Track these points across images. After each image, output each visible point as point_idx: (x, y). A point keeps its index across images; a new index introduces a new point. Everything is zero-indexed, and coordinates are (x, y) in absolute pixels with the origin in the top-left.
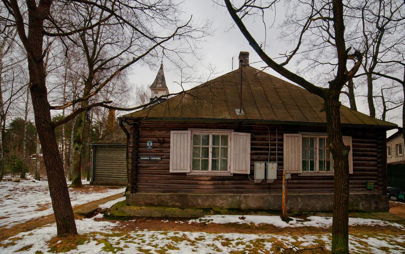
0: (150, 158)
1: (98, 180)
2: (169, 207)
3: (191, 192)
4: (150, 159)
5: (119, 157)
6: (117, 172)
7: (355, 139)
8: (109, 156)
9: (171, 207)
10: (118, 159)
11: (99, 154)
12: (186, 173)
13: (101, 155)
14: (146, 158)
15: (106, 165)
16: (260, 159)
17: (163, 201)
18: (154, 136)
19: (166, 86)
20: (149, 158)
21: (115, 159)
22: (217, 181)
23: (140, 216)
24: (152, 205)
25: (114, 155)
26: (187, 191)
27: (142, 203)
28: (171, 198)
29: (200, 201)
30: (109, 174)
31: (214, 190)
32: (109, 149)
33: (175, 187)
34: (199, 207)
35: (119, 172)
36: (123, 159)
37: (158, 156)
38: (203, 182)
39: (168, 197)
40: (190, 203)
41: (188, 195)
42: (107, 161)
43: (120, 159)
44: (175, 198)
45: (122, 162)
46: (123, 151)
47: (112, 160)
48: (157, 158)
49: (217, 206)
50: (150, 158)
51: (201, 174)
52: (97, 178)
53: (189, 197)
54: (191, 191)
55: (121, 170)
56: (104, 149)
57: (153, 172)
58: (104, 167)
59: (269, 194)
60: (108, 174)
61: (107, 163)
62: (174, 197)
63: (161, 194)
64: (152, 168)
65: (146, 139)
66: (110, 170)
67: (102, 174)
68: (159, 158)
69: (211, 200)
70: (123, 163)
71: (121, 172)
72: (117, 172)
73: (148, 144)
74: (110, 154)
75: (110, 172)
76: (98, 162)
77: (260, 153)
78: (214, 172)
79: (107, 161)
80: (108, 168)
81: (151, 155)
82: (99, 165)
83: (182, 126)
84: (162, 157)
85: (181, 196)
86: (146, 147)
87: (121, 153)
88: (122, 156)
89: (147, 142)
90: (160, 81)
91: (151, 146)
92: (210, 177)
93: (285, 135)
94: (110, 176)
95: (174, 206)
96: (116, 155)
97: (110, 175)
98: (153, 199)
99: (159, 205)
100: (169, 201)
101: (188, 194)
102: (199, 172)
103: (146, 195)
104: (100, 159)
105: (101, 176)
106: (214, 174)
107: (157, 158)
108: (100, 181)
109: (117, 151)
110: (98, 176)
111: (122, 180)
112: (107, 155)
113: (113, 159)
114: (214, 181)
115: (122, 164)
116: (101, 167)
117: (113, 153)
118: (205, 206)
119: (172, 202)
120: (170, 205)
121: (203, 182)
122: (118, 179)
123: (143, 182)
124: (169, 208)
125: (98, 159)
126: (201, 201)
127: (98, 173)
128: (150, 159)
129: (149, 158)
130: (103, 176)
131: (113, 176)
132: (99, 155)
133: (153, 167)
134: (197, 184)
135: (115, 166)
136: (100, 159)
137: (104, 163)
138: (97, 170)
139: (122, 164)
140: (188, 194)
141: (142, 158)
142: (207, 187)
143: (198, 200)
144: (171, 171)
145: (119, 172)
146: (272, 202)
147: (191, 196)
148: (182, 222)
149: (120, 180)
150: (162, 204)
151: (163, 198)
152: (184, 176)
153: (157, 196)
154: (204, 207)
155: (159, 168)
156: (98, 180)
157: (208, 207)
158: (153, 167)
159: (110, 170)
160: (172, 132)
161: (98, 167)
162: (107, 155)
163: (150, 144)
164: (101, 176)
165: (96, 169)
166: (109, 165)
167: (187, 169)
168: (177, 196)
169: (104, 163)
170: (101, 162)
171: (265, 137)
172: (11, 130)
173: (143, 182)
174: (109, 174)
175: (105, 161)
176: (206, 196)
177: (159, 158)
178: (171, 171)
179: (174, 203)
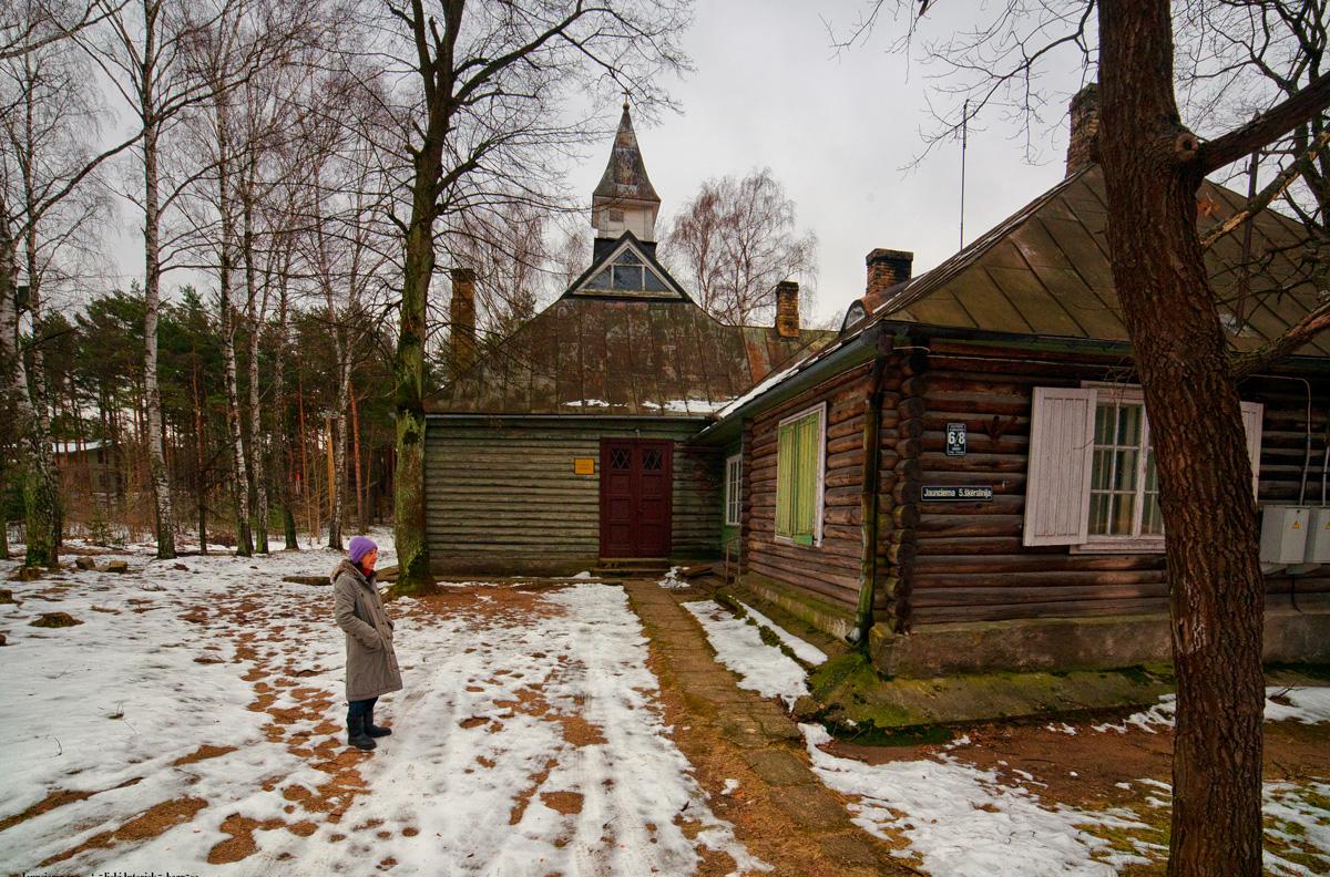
0: (957, 493)
1: (439, 554)
2: (1018, 671)
3: (1080, 612)
4: (957, 496)
5: (518, 466)
6: (515, 523)
7: (1277, 416)
8: (480, 462)
9: (1025, 672)
10: (517, 474)
11: (439, 453)
12: (1068, 546)
13: (448, 458)
14: (944, 493)
15: (467, 497)
16: (1276, 493)
17: (1001, 654)
18: (972, 407)
19: (652, 192)
20: (953, 494)
21: (502, 474)
22: (1149, 573)
23: (968, 718)
24: (964, 670)
25: (501, 459)
26: (1067, 610)
27: (932, 666)
28: (1027, 638)
29: (1110, 642)
30: (485, 531)
31: (1141, 601)
32: (480, 433)
33: (1030, 599)
34: (1106, 664)
35: (521, 523)
36: (535, 475)
37: (983, 483)
38: (1110, 576)
39: (1018, 637)
40: (1081, 654)
41: (1077, 625)
42: (473, 481)
43: (525, 474)
44: (1039, 639)
45: (529, 483)
46: (534, 444)
47: (492, 478)
48: (980, 493)
49: (1156, 658)
50: (957, 493)
51: (1112, 547)
52: (436, 546)
53: (1079, 633)
54: (1078, 610)
55: (529, 515)
56: (458, 435)
57: (966, 544)
58: (462, 507)
59: (1292, 613)
60: (477, 531)
61: (474, 490)
62: (1036, 637)
63: (993, 625)
64: (961, 531)
65: (941, 415)
66: (487, 515)
67: (456, 530)
68: (987, 494)
69: (1140, 638)
70: (534, 487)
71: (529, 523)
72: (515, 523)
73: (951, 440)
74: (482, 453)
75: (487, 523)
76: (437, 484)
77: (1274, 472)
78: (1148, 542)
79: (473, 481)
80: (479, 510)
81: (962, 482)
82: (443, 497)
83: (1068, 371)
84: (997, 487)
85: (1056, 628)
86: (943, 447)
87: (526, 450)
88: (530, 463)
89: (945, 430)
90: (627, 173)
91: (962, 446)
92: (1134, 558)
93: (1040, 395)
94: (488, 539)
95: (1033, 668)
96: (508, 458)
97: (486, 535)
98: (971, 649)
99: (988, 669)
100: (1021, 650)
101: (1075, 620)
102: (1106, 542)
103: (947, 635)
104: (442, 473)
105: (453, 539)
106: (1150, 547)
107: (980, 493)
108: (449, 557)
109: (512, 444)
110: (439, 538)
111: (533, 553)
112: (471, 457)
113: (497, 474)
114: (1142, 573)
115: (532, 490)
116: (451, 507)
117: (494, 450)
118: (1122, 659)
119: (1029, 652)
120: (1021, 663)
121: (1110, 576)
122: (517, 548)
123: (925, 583)
124: (1021, 676)
125: (434, 473)
126: (1115, 642)
127: (439, 530)
128: (957, 496)
129: (953, 494)
130: (461, 538)
131: (498, 540)
132: (441, 458)
133: (964, 525)
134: (1093, 583)
135: (506, 499)
136: (442, 473)
137: (462, 490)
138: (434, 518)
139: (532, 490)
140: (1075, 620)
141: (930, 493)
142: (1120, 594)
143: (1104, 642)
144: (1029, 541)
145: (521, 523)
146: (1307, 637)
147: (1087, 626)
148: (1070, 730)
149: (526, 553)
150: (998, 662)
151: (1003, 643)
152: (1059, 557)
153: (987, 634)
154: (1120, 665)
155: (984, 531)
156: (439, 554)
157: (1131, 661)
158: (966, 527)
159: (487, 515)
160: (1040, 395)
161: (438, 506)
162: (471, 457)
163: (956, 437)
164: (453, 539)
165: (432, 514)
166: (479, 498)
167: (1077, 535)
168: (1045, 632)
169: (462, 490)
170: (449, 485)
171: (1296, 417)
172: (36, 341)
173: (925, 583)
174: (485, 531)
175: (463, 481)
176: (1130, 624)
177: (987, 494)
178: (1029, 541)
179: (1033, 656)
